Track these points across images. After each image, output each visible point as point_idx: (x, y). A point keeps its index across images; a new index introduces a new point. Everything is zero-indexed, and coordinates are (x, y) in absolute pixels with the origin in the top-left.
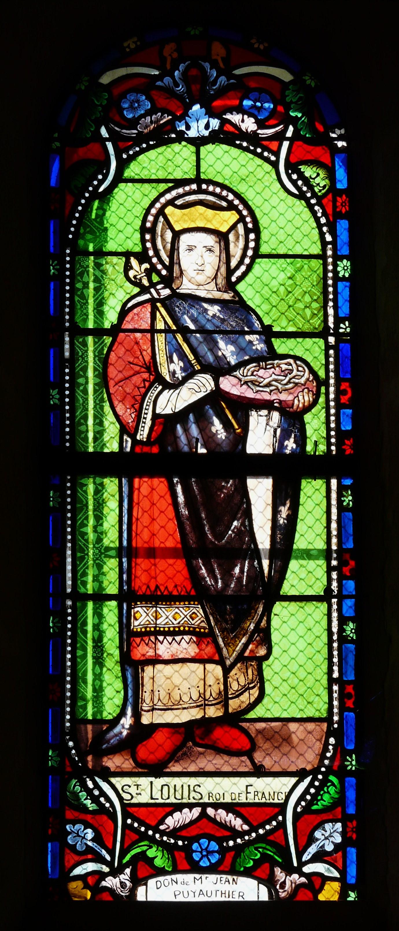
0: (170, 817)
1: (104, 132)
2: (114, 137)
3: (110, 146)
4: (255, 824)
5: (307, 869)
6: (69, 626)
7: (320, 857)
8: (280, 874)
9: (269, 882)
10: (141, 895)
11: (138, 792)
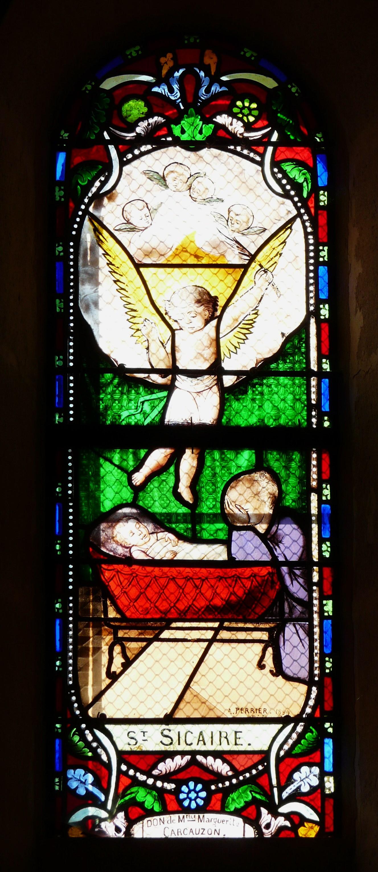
1: (106, 136)
3: (112, 149)
7: (297, 796)
8: (266, 817)
9: (253, 821)
11: (145, 738)
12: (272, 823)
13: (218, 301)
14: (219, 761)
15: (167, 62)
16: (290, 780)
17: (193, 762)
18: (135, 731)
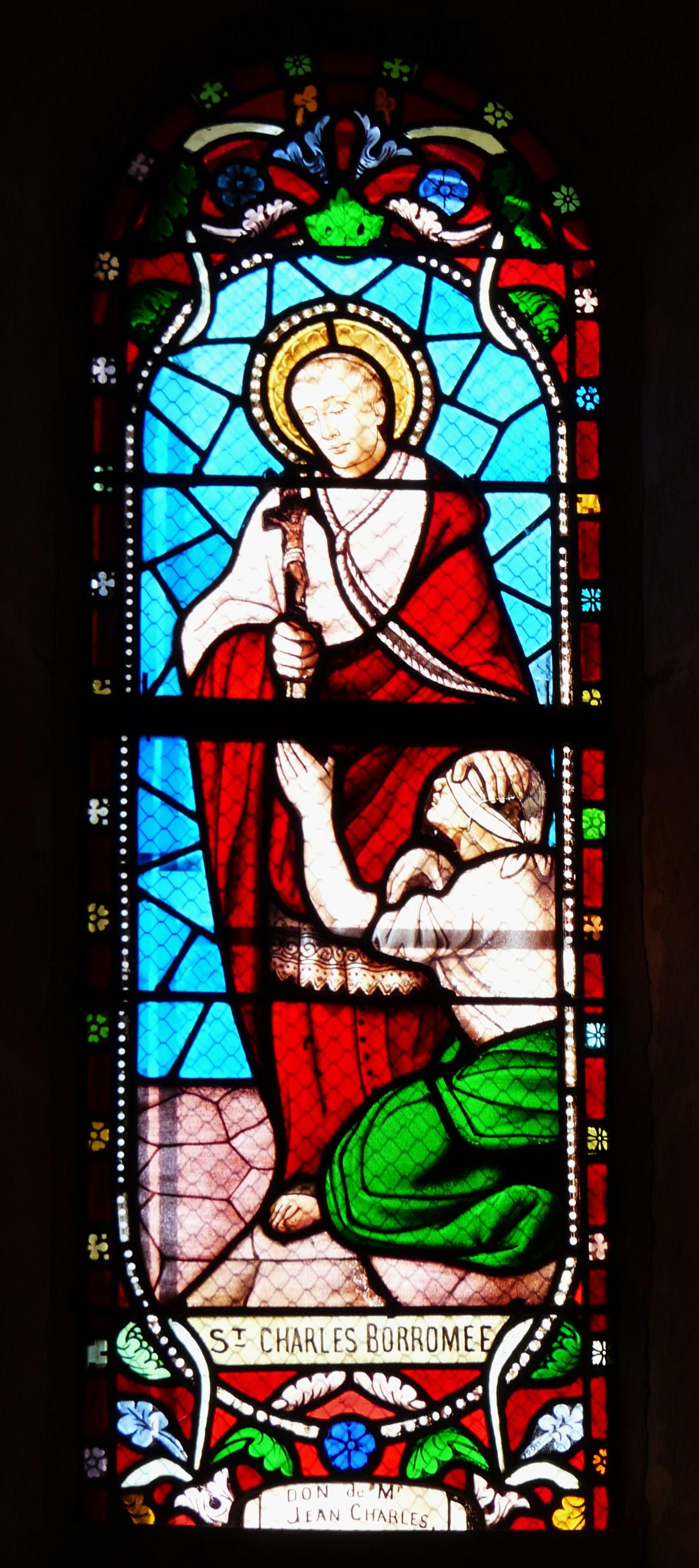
0: (291, 1387)
1: (191, 239)
3: (198, 257)
4: (436, 1397)
5: (518, 1477)
7: (548, 1455)
9: (463, 1494)
10: (251, 1519)
11: (241, 1342)
14: (395, 1381)
16: (532, 1431)
17: (349, 1385)
18: (221, 1328)
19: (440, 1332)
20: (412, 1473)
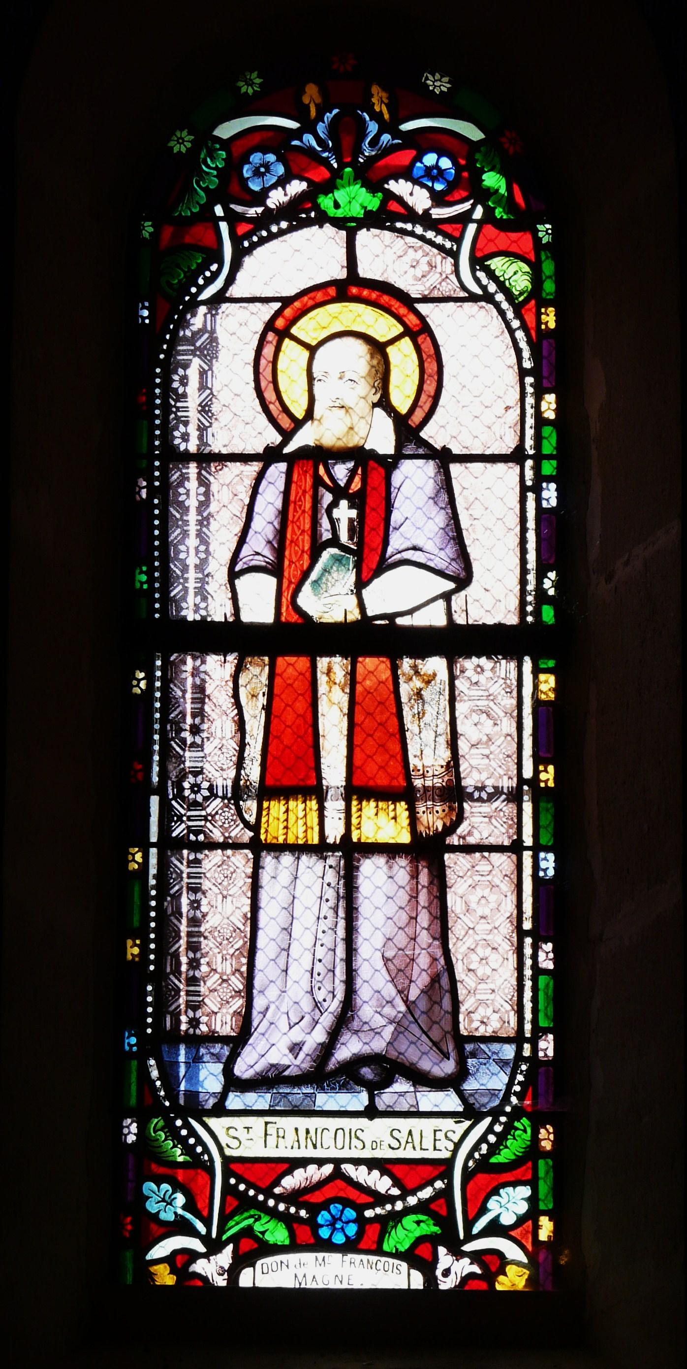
1: (219, 211)
2: (233, 218)
3: (224, 226)
6: (152, 946)
7: (495, 1229)
8: (445, 1259)
9: (427, 1266)
12: (453, 1270)
13: (368, 230)
14: (376, 1173)
15: (311, 95)
16: (483, 1210)
17: (337, 1174)
19: (319, 1145)
20: (388, 1246)
